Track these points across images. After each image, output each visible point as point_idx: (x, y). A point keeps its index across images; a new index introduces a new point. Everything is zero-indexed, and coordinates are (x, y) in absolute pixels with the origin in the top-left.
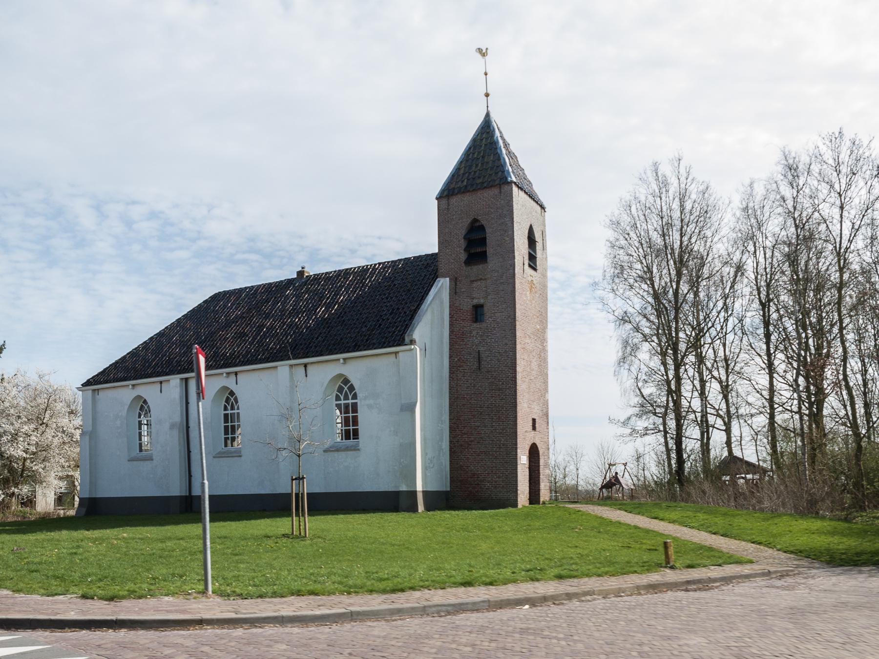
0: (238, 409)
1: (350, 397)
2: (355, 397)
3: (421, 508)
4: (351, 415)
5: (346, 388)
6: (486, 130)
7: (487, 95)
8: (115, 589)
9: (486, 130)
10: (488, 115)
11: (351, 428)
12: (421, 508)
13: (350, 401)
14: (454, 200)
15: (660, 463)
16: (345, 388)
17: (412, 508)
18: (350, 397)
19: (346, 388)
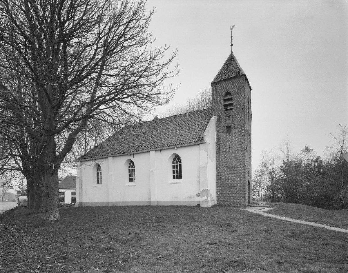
0: (134, 167)
1: (175, 163)
2: (180, 162)
3: (180, 164)
4: (179, 169)
5: (177, 159)
6: (231, 60)
7: (232, 37)
8: (246, 108)
9: (231, 60)
10: (232, 52)
11: (179, 169)
12: (180, 164)
13: (178, 164)
14: (219, 85)
15: (100, 169)
16: (177, 159)
17: (181, 165)
18: (175, 163)
19: (177, 159)
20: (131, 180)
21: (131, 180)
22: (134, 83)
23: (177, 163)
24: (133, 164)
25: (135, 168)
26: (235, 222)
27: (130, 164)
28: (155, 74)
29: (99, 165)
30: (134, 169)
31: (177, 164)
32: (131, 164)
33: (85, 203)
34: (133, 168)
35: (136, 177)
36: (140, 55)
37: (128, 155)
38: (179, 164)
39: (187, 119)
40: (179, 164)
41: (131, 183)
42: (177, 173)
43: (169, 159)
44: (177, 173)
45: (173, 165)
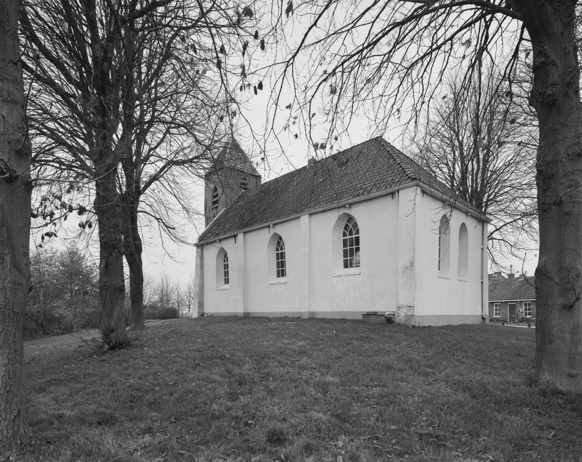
1: (354, 233)
20: (281, 273)
21: (281, 273)
22: (35, 154)
23: (351, 234)
24: (355, 225)
25: (361, 235)
26: (67, 413)
27: (346, 227)
28: (365, 88)
29: (281, 238)
30: (227, 264)
31: (352, 236)
32: (279, 242)
33: (320, 312)
34: (226, 263)
35: (288, 268)
36: (252, 75)
37: (345, 205)
38: (350, 237)
39: (368, 167)
40: (350, 237)
41: (282, 280)
42: (351, 249)
43: (218, 255)
44: (351, 249)
45: (344, 240)
